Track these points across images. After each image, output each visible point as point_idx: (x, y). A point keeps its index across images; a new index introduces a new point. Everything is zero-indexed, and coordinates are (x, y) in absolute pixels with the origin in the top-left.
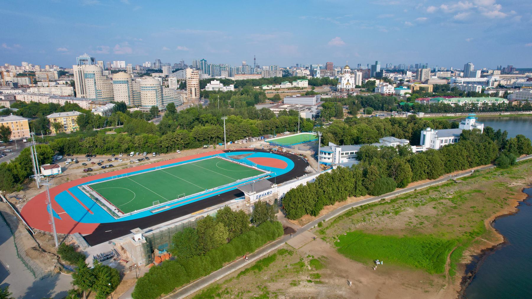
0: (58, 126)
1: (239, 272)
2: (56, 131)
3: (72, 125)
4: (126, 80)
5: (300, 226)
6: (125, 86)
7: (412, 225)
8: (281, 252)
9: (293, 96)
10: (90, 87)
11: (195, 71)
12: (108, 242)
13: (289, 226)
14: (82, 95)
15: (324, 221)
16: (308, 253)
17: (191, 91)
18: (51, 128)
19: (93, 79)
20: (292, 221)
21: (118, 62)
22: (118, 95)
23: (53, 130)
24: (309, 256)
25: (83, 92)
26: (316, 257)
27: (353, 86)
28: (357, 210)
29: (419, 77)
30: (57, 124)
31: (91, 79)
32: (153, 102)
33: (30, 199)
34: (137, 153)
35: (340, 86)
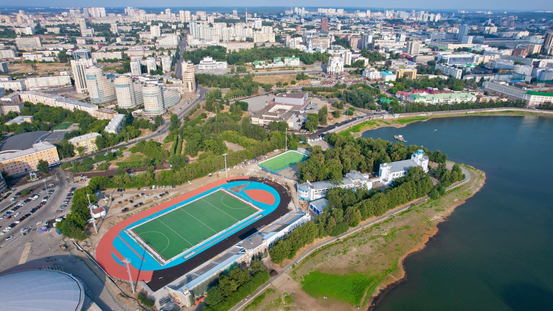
0: (81, 149)
1: (244, 308)
2: (80, 153)
3: (91, 145)
4: (128, 83)
5: (281, 269)
6: (126, 89)
7: (352, 264)
8: (269, 290)
9: (284, 96)
10: (92, 88)
11: (190, 65)
12: (163, 288)
13: (274, 269)
14: (82, 89)
15: (296, 263)
16: (284, 291)
17: (188, 84)
18: (75, 151)
19: (95, 80)
20: (276, 265)
21: (97, 8)
22: (122, 98)
23: (77, 152)
24: (285, 294)
25: (83, 86)
26: (289, 294)
27: (341, 70)
28: (320, 250)
29: (409, 50)
30: (80, 147)
31: (93, 80)
32: (156, 107)
33: (96, 246)
34: (158, 186)
35: (329, 69)
